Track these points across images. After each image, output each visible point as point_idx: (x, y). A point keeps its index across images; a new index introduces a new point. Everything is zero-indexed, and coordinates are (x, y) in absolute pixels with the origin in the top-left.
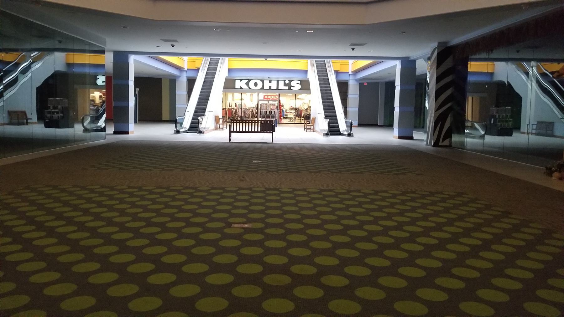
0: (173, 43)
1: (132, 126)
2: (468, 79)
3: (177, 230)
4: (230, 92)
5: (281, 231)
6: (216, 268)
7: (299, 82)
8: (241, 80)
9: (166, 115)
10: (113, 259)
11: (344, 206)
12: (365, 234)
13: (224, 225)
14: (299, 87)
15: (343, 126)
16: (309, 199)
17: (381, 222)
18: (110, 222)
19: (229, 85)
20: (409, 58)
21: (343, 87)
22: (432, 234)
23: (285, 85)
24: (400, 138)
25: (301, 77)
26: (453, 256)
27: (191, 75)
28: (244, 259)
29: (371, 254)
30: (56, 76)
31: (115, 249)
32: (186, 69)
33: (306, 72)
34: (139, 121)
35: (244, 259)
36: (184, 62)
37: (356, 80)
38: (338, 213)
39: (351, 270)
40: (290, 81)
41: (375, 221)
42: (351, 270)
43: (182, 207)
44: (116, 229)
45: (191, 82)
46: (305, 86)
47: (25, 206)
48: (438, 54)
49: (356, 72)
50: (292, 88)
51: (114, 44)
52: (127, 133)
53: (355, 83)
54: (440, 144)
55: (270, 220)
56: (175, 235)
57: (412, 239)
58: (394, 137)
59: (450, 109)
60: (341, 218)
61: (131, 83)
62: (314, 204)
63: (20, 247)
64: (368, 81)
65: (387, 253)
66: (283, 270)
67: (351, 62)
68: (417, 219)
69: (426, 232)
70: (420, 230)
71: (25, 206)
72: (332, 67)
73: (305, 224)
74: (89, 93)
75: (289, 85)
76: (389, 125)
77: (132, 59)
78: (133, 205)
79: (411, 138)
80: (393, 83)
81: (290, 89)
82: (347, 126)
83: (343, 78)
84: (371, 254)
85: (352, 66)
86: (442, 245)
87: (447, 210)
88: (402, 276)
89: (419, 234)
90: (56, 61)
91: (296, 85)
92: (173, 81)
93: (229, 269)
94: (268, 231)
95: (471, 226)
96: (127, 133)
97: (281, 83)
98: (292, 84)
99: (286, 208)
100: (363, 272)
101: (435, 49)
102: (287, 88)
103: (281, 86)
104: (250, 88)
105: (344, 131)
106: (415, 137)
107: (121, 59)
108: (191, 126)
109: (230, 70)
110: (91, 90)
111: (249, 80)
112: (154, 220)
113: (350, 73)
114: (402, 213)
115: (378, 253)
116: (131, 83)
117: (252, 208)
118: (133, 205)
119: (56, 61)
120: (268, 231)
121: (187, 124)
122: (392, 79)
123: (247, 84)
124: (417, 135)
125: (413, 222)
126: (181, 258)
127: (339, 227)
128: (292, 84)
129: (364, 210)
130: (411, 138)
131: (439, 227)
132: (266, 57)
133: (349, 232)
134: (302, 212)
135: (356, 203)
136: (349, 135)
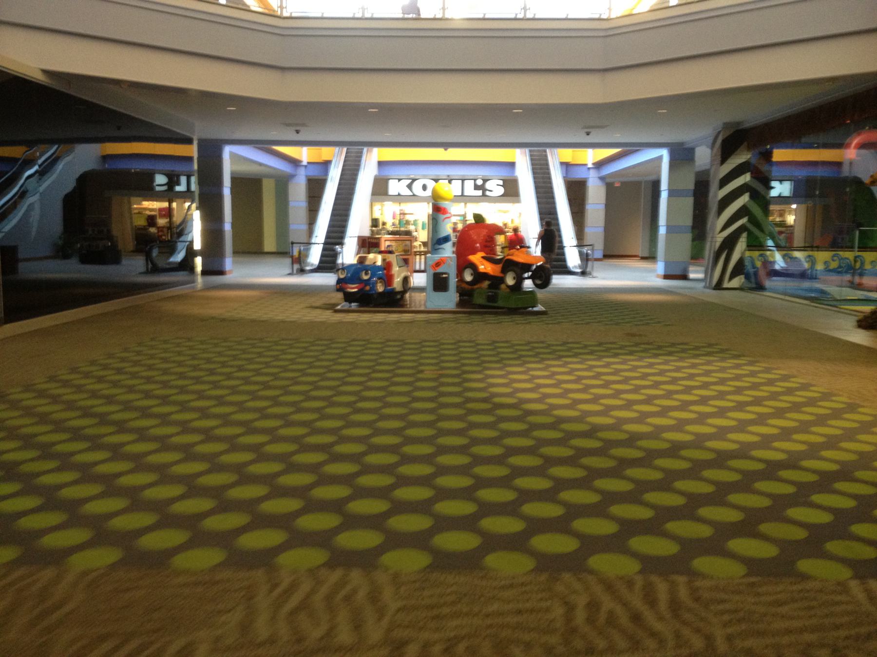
0: (298, 128)
1: (229, 263)
4: (379, 201)
5: (463, 482)
6: (353, 522)
7: (501, 182)
8: (399, 180)
9: (269, 244)
14: (501, 191)
15: (573, 258)
18: (139, 463)
19: (380, 190)
20: (682, 144)
21: (577, 191)
23: (477, 187)
24: (666, 277)
25: (504, 173)
27: (315, 172)
30: (84, 180)
32: (305, 163)
33: (512, 165)
34: (859, 248)
36: (304, 154)
37: (602, 179)
40: (485, 181)
45: (316, 188)
46: (511, 191)
48: (723, 141)
49: (599, 165)
50: (488, 193)
51: (203, 129)
52: (221, 273)
53: (599, 183)
54: (726, 285)
55: (444, 441)
58: (658, 276)
59: (742, 229)
61: (227, 192)
62: (530, 423)
64: (622, 179)
67: (590, 151)
72: (556, 158)
74: (130, 204)
75: (482, 187)
76: (651, 257)
77: (227, 151)
79: (684, 277)
80: (656, 184)
81: (484, 195)
82: (581, 259)
83: (579, 175)
85: (590, 156)
87: (757, 402)
88: (647, 505)
90: (85, 157)
91: (495, 188)
92: (283, 183)
93: (374, 522)
96: (221, 273)
97: (469, 185)
98: (488, 185)
101: (719, 133)
102: (480, 193)
103: (470, 190)
104: (414, 195)
105: (575, 267)
106: (692, 276)
107: (211, 153)
108: (321, 262)
109: (381, 164)
110: (133, 199)
111: (414, 180)
113: (590, 166)
116: (227, 192)
119: (85, 157)
121: (315, 256)
122: (653, 178)
123: (410, 186)
124: (696, 273)
126: (291, 505)
128: (488, 185)
130: (684, 277)
132: (446, 145)
136: (583, 273)
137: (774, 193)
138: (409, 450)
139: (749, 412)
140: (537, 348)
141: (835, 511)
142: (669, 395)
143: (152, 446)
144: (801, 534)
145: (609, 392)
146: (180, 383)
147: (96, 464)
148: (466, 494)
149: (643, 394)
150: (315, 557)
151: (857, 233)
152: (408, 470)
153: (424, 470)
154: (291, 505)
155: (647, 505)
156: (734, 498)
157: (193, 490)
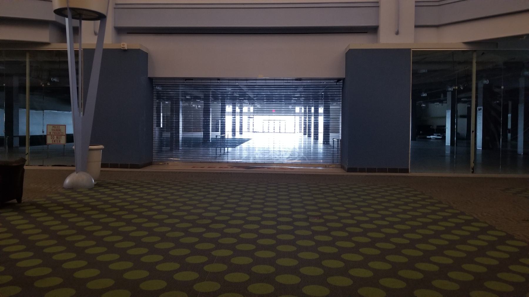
2: (202, 135)
3: (190, 246)
10: (144, 259)
11: (361, 230)
12: (368, 240)
13: (232, 253)
16: (326, 229)
17: (384, 230)
18: (126, 237)
22: (431, 241)
26: (450, 261)
28: (258, 261)
29: (366, 245)
31: (145, 250)
35: (258, 261)
38: (339, 214)
39: (347, 256)
41: (378, 229)
42: (347, 256)
43: (190, 230)
44: (146, 233)
47: (66, 213)
56: (197, 240)
57: (412, 244)
60: (347, 225)
63: (83, 237)
65: (389, 258)
66: (293, 270)
68: (407, 220)
69: (425, 239)
70: (420, 237)
71: (66, 213)
73: (313, 231)
78: (160, 212)
84: (366, 245)
86: (440, 251)
88: (401, 278)
89: (419, 241)
94: (280, 237)
95: (467, 233)
99: (295, 216)
100: (357, 258)
112: (186, 218)
114: (403, 222)
115: (381, 258)
117: (265, 209)
118: (160, 212)
120: (280, 237)
125: (413, 230)
126: (192, 276)
127: (345, 234)
129: (362, 212)
131: (437, 235)
133: (347, 229)
134: (320, 249)
135: (367, 219)
137: (230, 137)
138: (261, 242)
139: (428, 218)
140: (329, 196)
141: (488, 266)
142: (394, 215)
143: (120, 238)
144: (470, 278)
145: (350, 201)
146: (157, 199)
147: (87, 248)
148: (292, 255)
149: (373, 208)
150: (215, 286)
151: (161, 126)
152: (261, 254)
153: (270, 254)
154: (192, 276)
155: (401, 278)
156: (433, 259)
157: (153, 251)
